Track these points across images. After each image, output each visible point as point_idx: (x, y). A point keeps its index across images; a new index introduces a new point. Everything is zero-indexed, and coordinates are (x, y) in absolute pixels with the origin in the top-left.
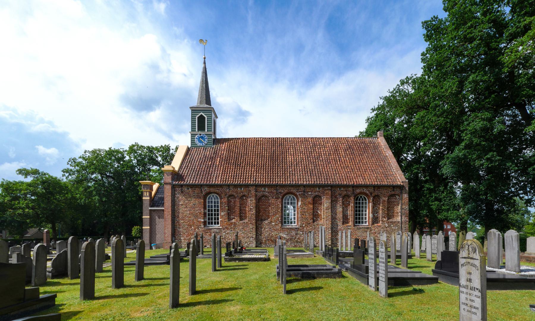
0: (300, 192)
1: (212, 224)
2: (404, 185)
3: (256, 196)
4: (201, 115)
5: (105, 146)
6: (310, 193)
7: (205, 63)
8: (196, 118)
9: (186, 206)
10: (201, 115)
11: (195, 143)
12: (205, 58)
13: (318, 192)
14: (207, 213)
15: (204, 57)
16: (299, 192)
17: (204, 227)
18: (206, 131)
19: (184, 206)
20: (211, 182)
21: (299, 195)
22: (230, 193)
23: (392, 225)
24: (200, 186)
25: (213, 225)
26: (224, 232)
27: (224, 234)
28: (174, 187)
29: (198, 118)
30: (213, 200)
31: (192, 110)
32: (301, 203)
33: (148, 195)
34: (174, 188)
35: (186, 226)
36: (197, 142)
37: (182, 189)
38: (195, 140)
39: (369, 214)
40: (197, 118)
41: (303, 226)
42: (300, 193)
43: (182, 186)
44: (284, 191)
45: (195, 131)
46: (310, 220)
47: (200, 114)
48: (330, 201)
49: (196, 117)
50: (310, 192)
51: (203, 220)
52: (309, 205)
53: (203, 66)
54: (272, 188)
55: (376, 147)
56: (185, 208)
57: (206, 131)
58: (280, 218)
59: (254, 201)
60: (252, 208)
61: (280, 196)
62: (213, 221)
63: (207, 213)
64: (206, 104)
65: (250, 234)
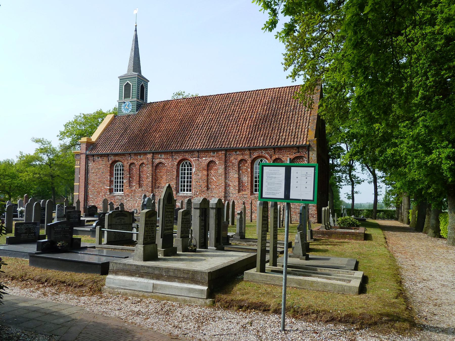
0: (195, 157)
1: (184, 191)
2: (311, 144)
3: (153, 163)
5: (72, 119)
6: (204, 159)
7: (136, 31)
12: (136, 26)
13: (212, 157)
14: (114, 180)
15: (135, 25)
16: (194, 157)
19: (95, 174)
20: (301, 143)
21: (194, 161)
24: (107, 155)
25: (186, 192)
27: (126, 201)
28: (87, 157)
29: (125, 86)
30: (119, 168)
31: (120, 79)
32: (196, 170)
34: (87, 157)
35: (96, 193)
40: (131, 85)
41: (196, 194)
43: (93, 156)
48: (223, 166)
49: (123, 85)
51: (109, 187)
52: (204, 171)
53: (134, 33)
54: (167, 154)
59: (150, 169)
61: (175, 162)
63: (114, 180)
64: (133, 71)
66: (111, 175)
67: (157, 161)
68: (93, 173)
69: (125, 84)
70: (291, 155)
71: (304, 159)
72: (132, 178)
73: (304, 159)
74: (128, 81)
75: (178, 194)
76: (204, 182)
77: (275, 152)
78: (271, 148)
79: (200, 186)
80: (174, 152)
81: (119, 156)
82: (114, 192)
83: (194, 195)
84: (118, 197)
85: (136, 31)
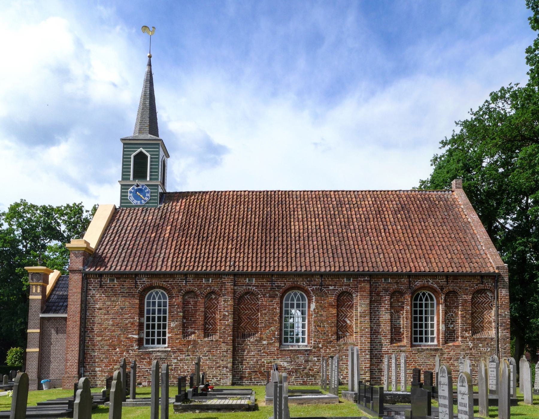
0: (315, 285)
1: (153, 343)
3: (234, 292)
4: (141, 153)
6: (331, 288)
7: (150, 65)
8: (130, 158)
9: (108, 312)
10: (141, 153)
11: (127, 199)
13: (345, 285)
14: (145, 323)
15: (149, 55)
16: (312, 285)
17: (139, 349)
18: (148, 179)
19: (103, 311)
21: (313, 290)
22: (188, 287)
23: (480, 345)
26: (175, 359)
27: (175, 361)
28: (86, 277)
31: (124, 144)
32: (316, 306)
33: (39, 291)
34: (87, 279)
36: (132, 198)
37: (101, 281)
38: (127, 196)
39: (438, 325)
40: (132, 157)
41: (318, 347)
42: (314, 287)
43: (101, 275)
44: (285, 284)
45: (129, 179)
46: (332, 335)
47: (139, 150)
48: (368, 301)
49: (131, 155)
50: (331, 285)
51: (136, 337)
52: (331, 309)
53: (146, 69)
54: (263, 278)
55: (450, 207)
56: (105, 314)
57: (148, 179)
58: (276, 333)
59: (231, 302)
60: (227, 314)
61: (277, 293)
62: (156, 338)
63: (145, 323)
65: (222, 360)
66: (141, 315)
67: (241, 290)
68: (100, 309)
69: (135, 154)
70: (472, 287)
71: (488, 293)
72: (187, 319)
73: (488, 293)
74: (141, 149)
75: (282, 346)
76: (332, 327)
77: (447, 281)
78: (443, 276)
79: (325, 333)
80: (277, 275)
81: (160, 278)
82: (145, 345)
83: (314, 348)
84: (159, 354)
85: (150, 65)
